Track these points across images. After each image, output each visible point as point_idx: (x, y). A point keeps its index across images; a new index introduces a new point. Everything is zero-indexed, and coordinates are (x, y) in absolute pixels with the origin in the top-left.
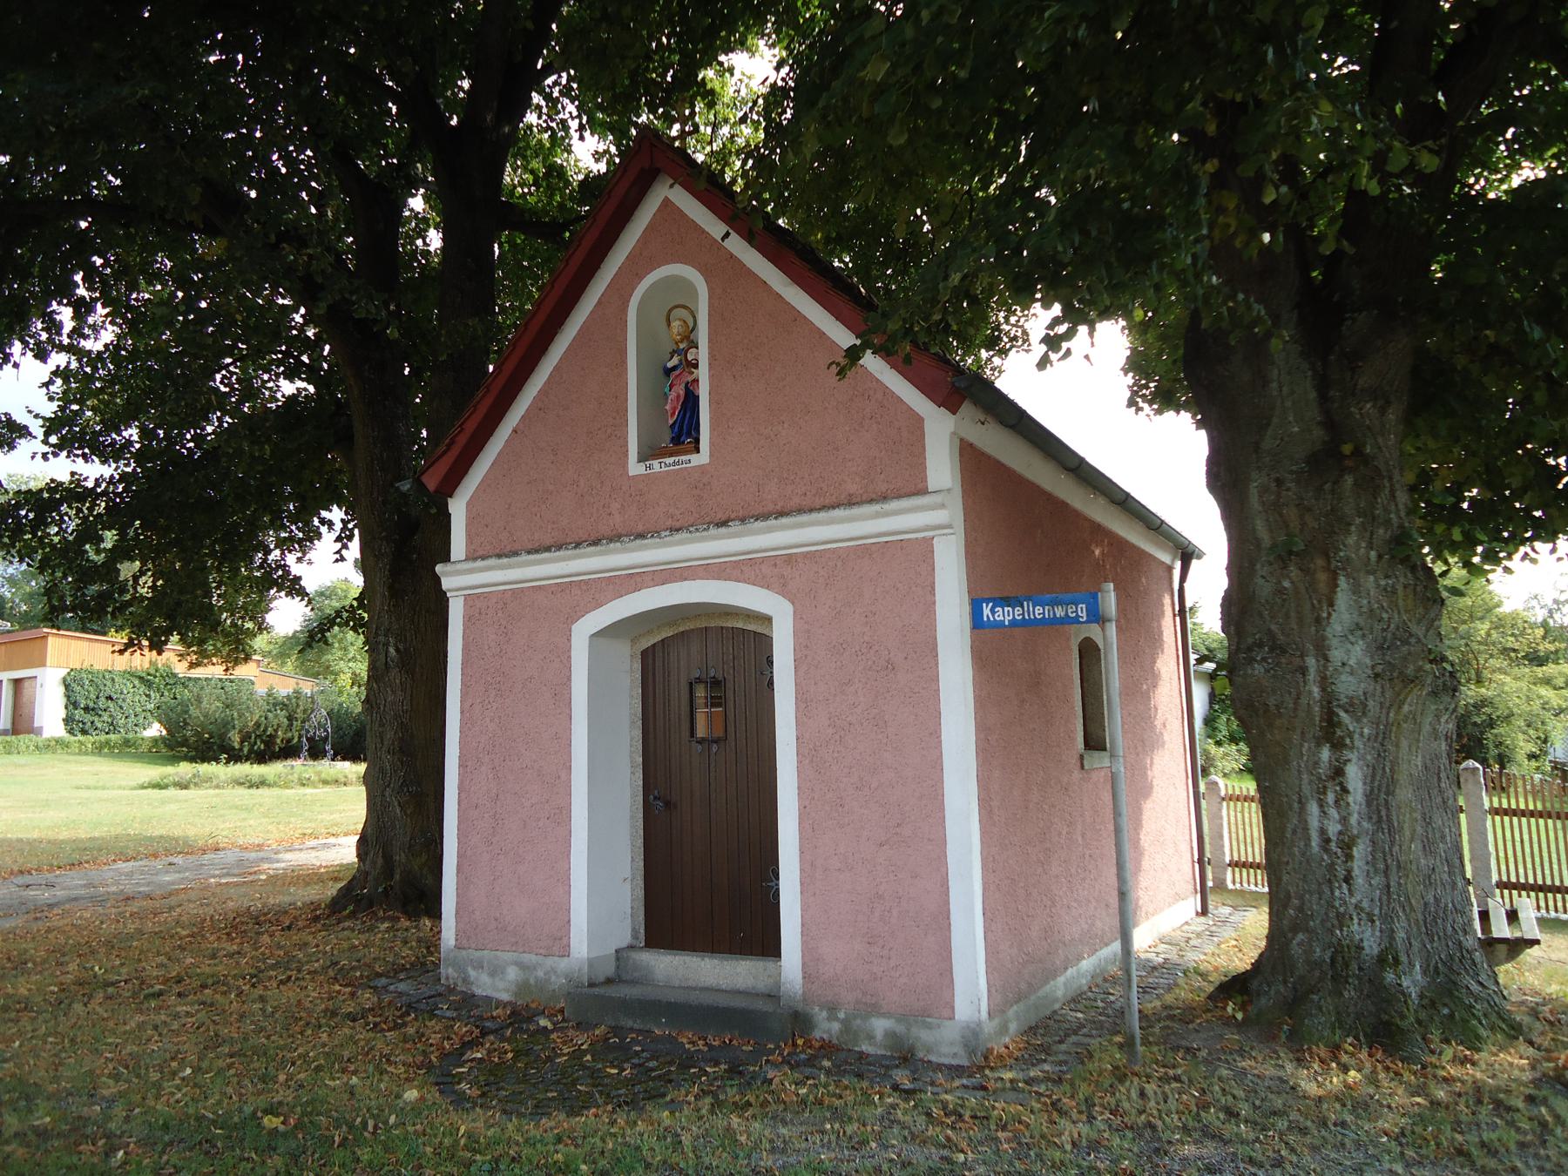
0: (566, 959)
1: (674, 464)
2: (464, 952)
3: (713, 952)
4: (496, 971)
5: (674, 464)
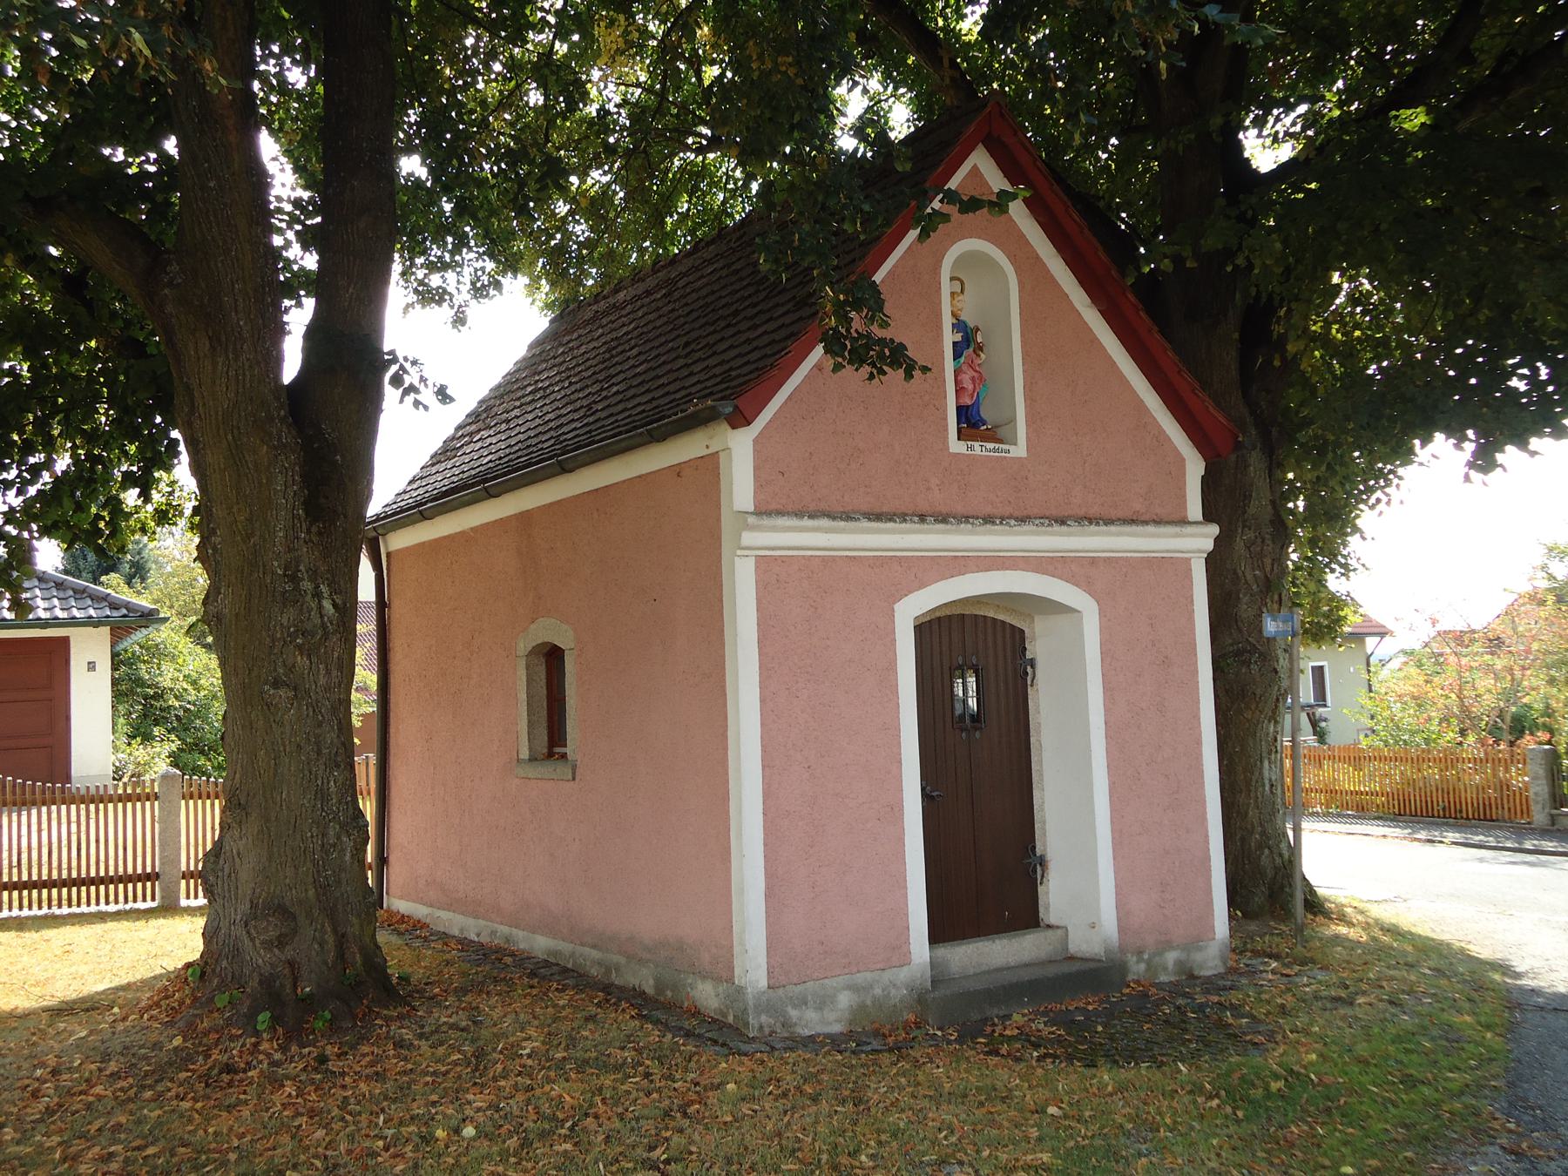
0: (905, 969)
2: (780, 992)
3: (944, 942)
4: (824, 1002)
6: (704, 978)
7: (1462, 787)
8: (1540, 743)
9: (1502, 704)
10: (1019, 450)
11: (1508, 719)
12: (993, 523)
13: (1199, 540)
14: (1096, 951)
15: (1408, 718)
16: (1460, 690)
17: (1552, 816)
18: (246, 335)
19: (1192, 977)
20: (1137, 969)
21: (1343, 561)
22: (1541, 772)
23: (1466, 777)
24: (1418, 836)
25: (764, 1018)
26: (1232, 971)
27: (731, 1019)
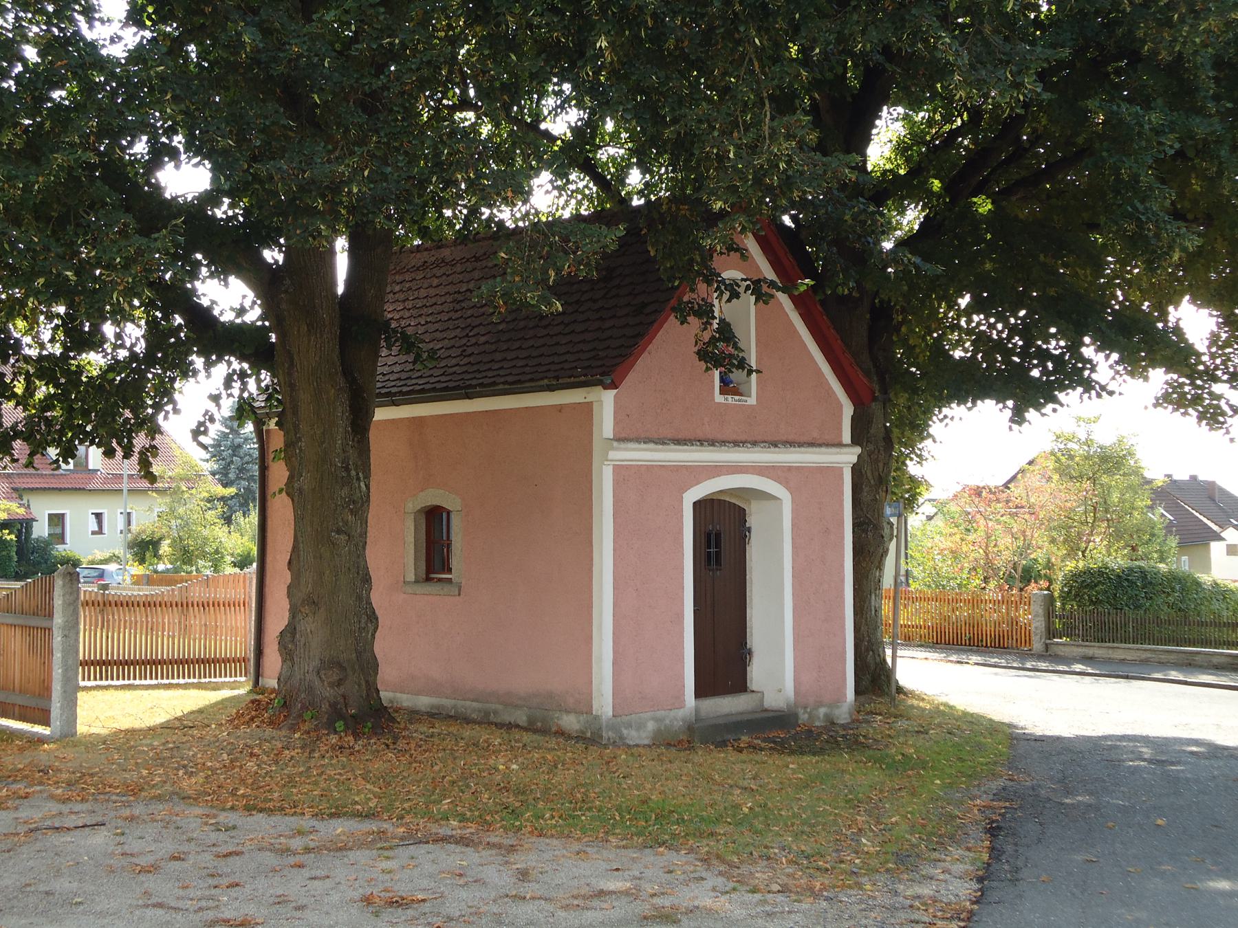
1: (739, 401)
2: (619, 719)
4: (640, 726)
5: (739, 401)
6: (568, 712)
7: (984, 623)
8: (1041, 589)
9: (1016, 558)
10: (752, 401)
11: (1020, 570)
12: (739, 446)
13: (848, 457)
14: (782, 705)
15: (945, 568)
16: (987, 546)
17: (1047, 645)
18: (327, 323)
19: (833, 723)
20: (803, 717)
21: (919, 452)
22: (1041, 611)
23: (988, 614)
24: (951, 659)
25: (610, 733)
26: (853, 721)
27: (589, 735)
